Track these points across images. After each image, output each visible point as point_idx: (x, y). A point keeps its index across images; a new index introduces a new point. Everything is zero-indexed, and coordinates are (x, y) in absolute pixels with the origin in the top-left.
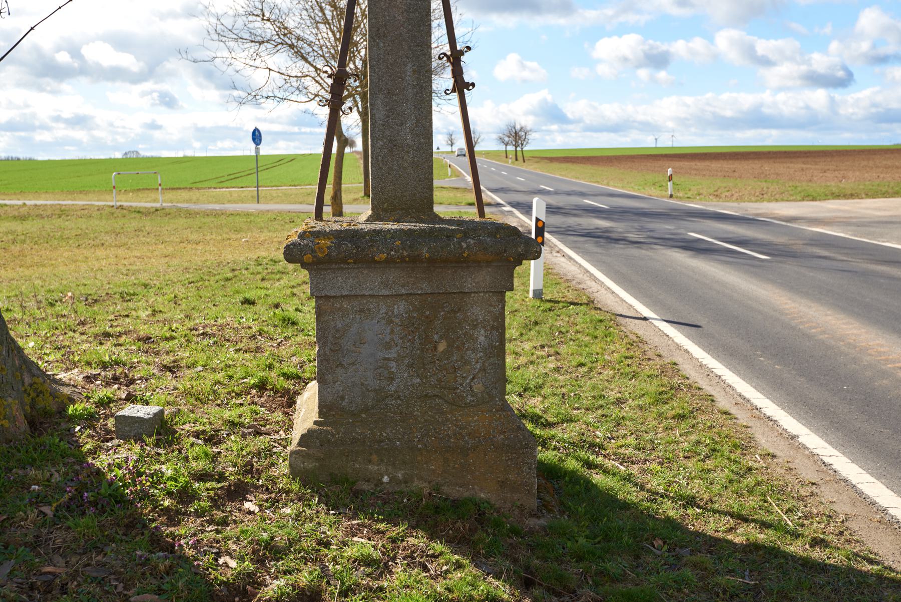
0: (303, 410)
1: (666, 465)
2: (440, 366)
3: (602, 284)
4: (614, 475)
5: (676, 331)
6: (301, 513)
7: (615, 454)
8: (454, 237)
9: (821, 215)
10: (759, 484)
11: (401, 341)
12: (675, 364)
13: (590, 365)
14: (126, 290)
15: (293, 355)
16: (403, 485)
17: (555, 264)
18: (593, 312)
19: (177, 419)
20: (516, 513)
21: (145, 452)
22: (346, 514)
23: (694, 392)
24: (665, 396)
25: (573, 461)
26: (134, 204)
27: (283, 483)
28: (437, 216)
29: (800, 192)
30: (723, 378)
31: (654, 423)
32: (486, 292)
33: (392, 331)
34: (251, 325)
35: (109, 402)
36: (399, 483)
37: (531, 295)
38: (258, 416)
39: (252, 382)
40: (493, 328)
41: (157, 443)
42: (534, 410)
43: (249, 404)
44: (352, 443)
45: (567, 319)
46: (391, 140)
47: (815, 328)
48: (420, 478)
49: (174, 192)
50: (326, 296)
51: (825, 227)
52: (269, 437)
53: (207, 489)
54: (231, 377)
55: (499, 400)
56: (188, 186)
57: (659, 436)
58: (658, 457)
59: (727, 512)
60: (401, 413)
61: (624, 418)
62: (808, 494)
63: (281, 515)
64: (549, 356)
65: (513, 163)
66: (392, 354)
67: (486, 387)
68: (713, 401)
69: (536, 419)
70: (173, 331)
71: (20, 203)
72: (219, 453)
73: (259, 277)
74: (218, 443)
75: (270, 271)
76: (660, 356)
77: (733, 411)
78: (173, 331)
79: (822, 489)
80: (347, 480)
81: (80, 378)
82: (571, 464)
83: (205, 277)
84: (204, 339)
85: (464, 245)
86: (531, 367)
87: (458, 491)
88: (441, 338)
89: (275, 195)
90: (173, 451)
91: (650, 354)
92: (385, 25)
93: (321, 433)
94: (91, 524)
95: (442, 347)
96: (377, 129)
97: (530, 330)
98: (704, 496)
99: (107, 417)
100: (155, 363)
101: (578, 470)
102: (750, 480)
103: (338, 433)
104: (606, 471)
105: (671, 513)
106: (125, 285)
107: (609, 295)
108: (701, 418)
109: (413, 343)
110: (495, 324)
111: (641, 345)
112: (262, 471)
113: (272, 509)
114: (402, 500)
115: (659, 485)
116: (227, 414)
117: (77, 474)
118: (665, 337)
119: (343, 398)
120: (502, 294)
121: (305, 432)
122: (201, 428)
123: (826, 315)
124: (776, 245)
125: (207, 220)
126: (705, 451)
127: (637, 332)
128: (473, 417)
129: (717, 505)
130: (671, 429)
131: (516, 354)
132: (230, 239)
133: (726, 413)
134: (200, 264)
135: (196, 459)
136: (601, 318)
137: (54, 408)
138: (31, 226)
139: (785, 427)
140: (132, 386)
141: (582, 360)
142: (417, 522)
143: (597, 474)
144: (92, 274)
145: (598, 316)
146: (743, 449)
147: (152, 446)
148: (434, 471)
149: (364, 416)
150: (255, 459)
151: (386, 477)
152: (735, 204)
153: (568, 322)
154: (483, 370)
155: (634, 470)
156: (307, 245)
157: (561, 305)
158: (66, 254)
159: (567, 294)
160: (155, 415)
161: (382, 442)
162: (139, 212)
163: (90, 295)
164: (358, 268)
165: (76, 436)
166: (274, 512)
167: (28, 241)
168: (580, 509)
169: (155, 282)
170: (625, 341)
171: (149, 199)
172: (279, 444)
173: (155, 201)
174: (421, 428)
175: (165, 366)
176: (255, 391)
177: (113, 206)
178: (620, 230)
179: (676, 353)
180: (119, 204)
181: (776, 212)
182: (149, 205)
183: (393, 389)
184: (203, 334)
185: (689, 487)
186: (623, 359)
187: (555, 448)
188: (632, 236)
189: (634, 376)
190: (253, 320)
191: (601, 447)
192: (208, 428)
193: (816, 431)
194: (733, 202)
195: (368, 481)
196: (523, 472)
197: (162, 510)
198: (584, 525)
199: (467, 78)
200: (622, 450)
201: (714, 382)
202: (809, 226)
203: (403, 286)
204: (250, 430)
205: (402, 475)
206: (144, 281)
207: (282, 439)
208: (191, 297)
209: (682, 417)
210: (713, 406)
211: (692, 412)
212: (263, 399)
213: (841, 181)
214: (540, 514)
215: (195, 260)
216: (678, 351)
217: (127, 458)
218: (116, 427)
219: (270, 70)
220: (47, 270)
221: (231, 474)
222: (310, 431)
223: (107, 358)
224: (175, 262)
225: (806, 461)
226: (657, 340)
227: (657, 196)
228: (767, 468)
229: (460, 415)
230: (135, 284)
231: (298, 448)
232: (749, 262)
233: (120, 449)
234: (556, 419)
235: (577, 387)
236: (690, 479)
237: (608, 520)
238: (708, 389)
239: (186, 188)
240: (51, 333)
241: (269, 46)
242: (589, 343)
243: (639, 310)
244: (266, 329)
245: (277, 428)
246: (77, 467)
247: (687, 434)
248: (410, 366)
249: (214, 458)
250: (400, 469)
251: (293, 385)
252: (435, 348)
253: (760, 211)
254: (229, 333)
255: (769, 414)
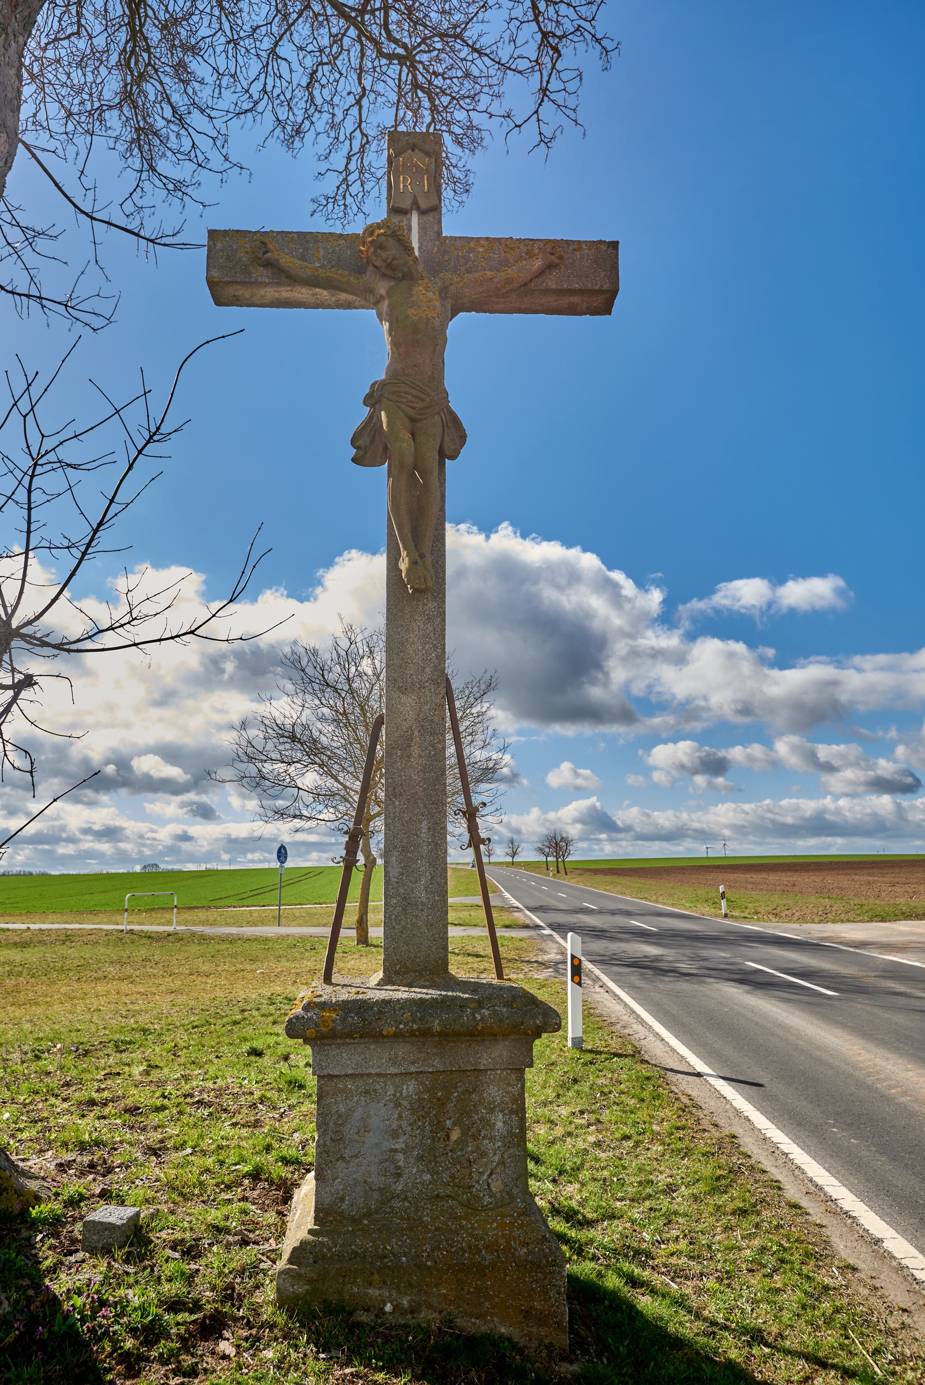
0: (299, 1212)
1: (726, 1282)
2: (453, 1159)
3: (650, 1028)
4: (663, 1296)
5: (734, 1092)
6: (284, 1358)
7: (665, 1266)
8: (468, 1007)
9: (893, 939)
10: (837, 1310)
11: (409, 1128)
12: (734, 1137)
13: (635, 1138)
14: (123, 1038)
15: (295, 1131)
16: (409, 1316)
17: (598, 1002)
18: (639, 1067)
19: (154, 1224)
20: (544, 1355)
21: (111, 1270)
22: (338, 1358)
23: (758, 1176)
24: (723, 1182)
25: (614, 1277)
26: (146, 928)
27: (267, 1313)
28: (453, 978)
29: (867, 912)
30: (791, 1156)
31: (712, 1220)
32: (504, 1069)
33: (400, 1117)
34: (253, 1088)
35: (80, 1201)
36: (404, 1312)
37: (569, 1044)
38: (248, 1218)
39: (246, 1169)
40: (512, 1112)
41: (127, 1257)
42: (570, 1202)
43: (239, 1200)
44: (350, 1259)
45: (610, 1076)
46: (405, 898)
47: (895, 1087)
48: (430, 1307)
49: (191, 912)
50: (329, 1075)
51: (898, 954)
52: (257, 1247)
53: (178, 1324)
54: (222, 1163)
55: (522, 1202)
56: (207, 905)
57: (718, 1238)
58: (716, 1270)
59: (800, 1353)
60: (409, 1218)
61: (675, 1213)
62: (897, 1326)
63: (261, 1360)
64: (589, 1125)
65: (554, 876)
66: (400, 1145)
67: (506, 1186)
68: (780, 1188)
69: (570, 1216)
70: (165, 1097)
71: (24, 927)
72: (198, 1270)
73: (271, 1019)
74: (199, 1256)
75: (283, 1012)
76: (716, 1125)
77: (804, 1203)
78: (165, 1097)
79: (916, 1319)
80: (344, 1309)
81: (52, 1166)
82: (612, 1282)
83: (212, 1020)
84: (198, 1108)
85: (478, 1017)
86: (569, 1139)
87: (475, 1324)
88: (454, 1124)
89: (297, 915)
90: (145, 1268)
91: (705, 1124)
92: (401, 785)
93: (315, 1246)
94: (35, 1376)
95: (455, 1135)
96: (391, 887)
97: (568, 1089)
98: (773, 1328)
99: (75, 1220)
100: (139, 1142)
101: (620, 1290)
102: (826, 1306)
103: (335, 1247)
104: (653, 1292)
105: (733, 1354)
106: (121, 1030)
107: (659, 1043)
108: (766, 1214)
109: (423, 1130)
110: (514, 1106)
111: (694, 1111)
112: (244, 1296)
113: (251, 1352)
114: (407, 1337)
115: (718, 1310)
116: (214, 1215)
117: (30, 1301)
118: (722, 1100)
119: (342, 1199)
120: (521, 1072)
121: (297, 1244)
122: (178, 1236)
123: (907, 1070)
124: (845, 977)
125: (223, 947)
126: (772, 1261)
127: (690, 1092)
128: (491, 1224)
129: (788, 1343)
130: (731, 1229)
131: (552, 1122)
132: (243, 970)
133: (796, 1206)
134: (208, 1003)
135: (170, 1280)
136: (648, 1074)
137: (17, 1208)
138: (32, 956)
139: (867, 1227)
140: (110, 1176)
141: (627, 1130)
142: (423, 1370)
143: (643, 1294)
144: (88, 1016)
145: (645, 1071)
146: (817, 1259)
147: (121, 1261)
148: (445, 1296)
149: (366, 1222)
150: (238, 1280)
151: (389, 1305)
152: (796, 926)
153: (611, 1079)
154: (502, 1163)
155: (688, 1288)
156: (311, 1018)
157: (603, 1056)
158: (63, 990)
159: (610, 1042)
160: (130, 1219)
161: (385, 1257)
162: (150, 937)
163: (81, 1043)
164: (364, 1043)
165: (36, 1248)
166: (253, 1355)
167: (25, 973)
168: (621, 1349)
169: (156, 1026)
170: (676, 1105)
171: (163, 920)
172: (268, 1257)
173: (169, 923)
174: (431, 1239)
175: (150, 1148)
176: (247, 1181)
177: (123, 931)
178: (670, 959)
179: (735, 1121)
180: (129, 927)
181: (843, 935)
182: (161, 929)
183: (400, 1188)
184: (198, 1102)
185: (754, 1315)
186: (673, 1130)
187: (594, 1258)
188: (683, 967)
189: (688, 1153)
190: (257, 1082)
191: (649, 1255)
192: (188, 1235)
193: (903, 1233)
194: (794, 922)
195: (368, 1310)
196: (550, 1298)
197: (120, 1355)
198: (626, 1373)
199: (483, 834)
200: (673, 1260)
201: (780, 1162)
202: (880, 954)
203: (413, 1063)
204: (237, 1238)
205: (409, 1302)
206: (143, 1025)
207: (273, 1251)
208: (194, 1046)
209: (743, 1213)
210: (779, 1196)
211: (755, 1205)
212: (256, 1192)
213: (911, 898)
214: (573, 1357)
215: (202, 997)
216: (737, 1118)
217: (90, 1280)
218: (84, 1235)
219: (299, 788)
220: (39, 1010)
221: (208, 1302)
222: (304, 1244)
223: (87, 1137)
224: (181, 999)
225: (894, 1276)
226: (713, 1104)
227: (710, 916)
228: (847, 1287)
229: (477, 1221)
230: (133, 1029)
231: (288, 1266)
232: (815, 1000)
233: (84, 1265)
234: (595, 1215)
235: (621, 1168)
236: (755, 1302)
237: (656, 1364)
238: (776, 1173)
239: (204, 907)
240: (31, 1098)
241: (299, 765)
242: (635, 1107)
243: (692, 1063)
244: (268, 1095)
245: (267, 1234)
246: (31, 1292)
247: (749, 1237)
248: (420, 1158)
249: (190, 1279)
250: (406, 1294)
251: (292, 1173)
252: (448, 1136)
253: (825, 935)
254: (227, 1102)
255: (846, 1207)
